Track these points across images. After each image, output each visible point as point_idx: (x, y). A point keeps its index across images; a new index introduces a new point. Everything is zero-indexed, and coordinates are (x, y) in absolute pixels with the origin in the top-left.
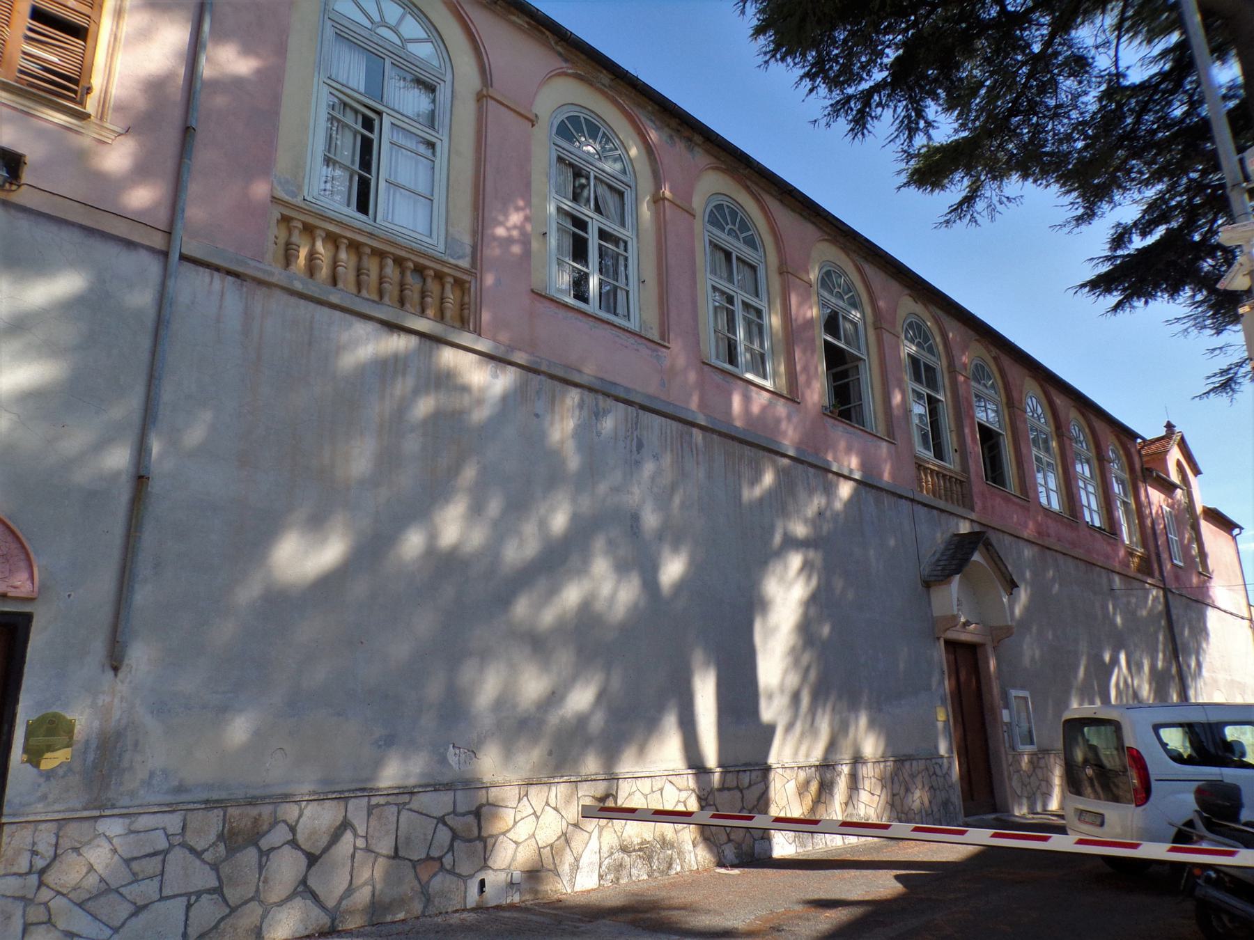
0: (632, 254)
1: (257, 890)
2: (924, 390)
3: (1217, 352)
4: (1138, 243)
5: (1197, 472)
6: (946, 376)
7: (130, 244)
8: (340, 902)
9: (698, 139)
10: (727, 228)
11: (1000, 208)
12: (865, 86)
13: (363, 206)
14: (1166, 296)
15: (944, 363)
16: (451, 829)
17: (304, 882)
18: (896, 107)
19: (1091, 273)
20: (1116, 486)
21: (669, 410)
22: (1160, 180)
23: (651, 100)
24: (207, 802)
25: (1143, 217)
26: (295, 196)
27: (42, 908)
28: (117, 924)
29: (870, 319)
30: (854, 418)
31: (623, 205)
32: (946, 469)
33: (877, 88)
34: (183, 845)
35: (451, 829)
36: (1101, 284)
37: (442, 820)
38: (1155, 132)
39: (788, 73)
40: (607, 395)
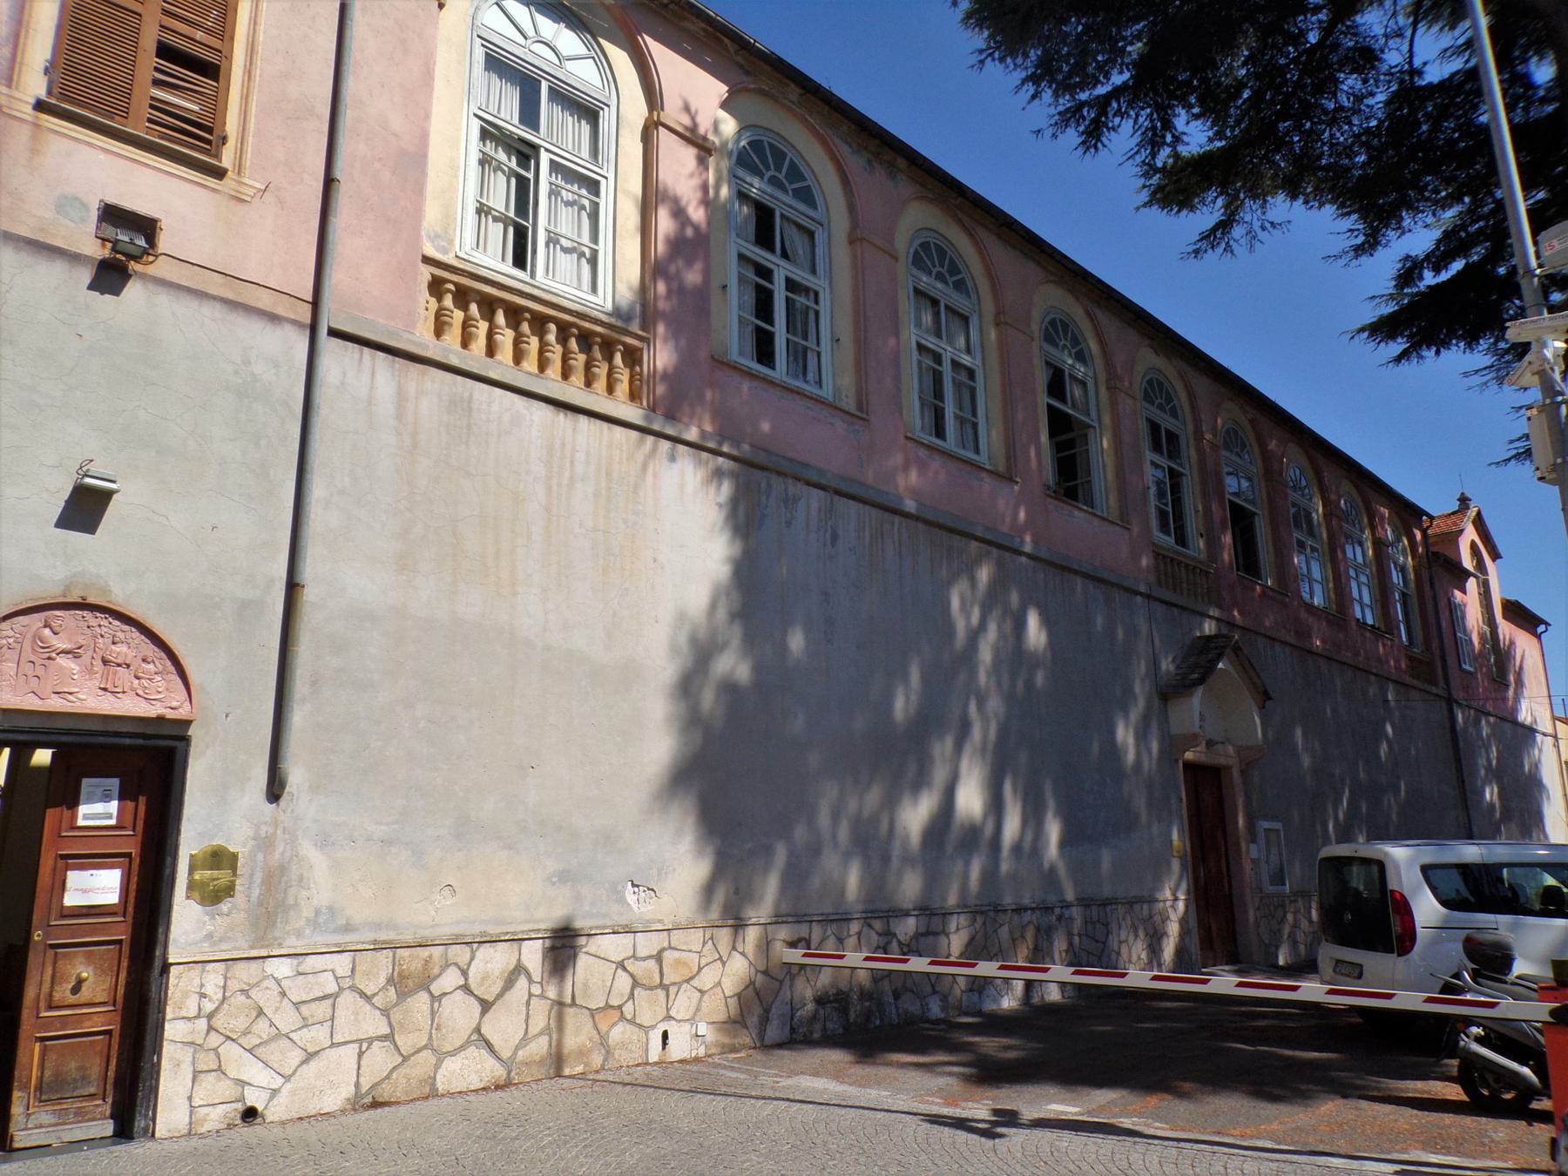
0: (824, 307)
1: (430, 1038)
2: (1164, 462)
4: (1429, 279)
6: (1192, 442)
7: (274, 318)
8: (515, 1053)
9: (901, 163)
10: (934, 271)
11: (1261, 235)
12: (1101, 90)
13: (520, 261)
14: (1462, 344)
15: (1190, 427)
16: (632, 975)
17: (478, 1030)
18: (1137, 116)
19: (1371, 313)
20: (1394, 573)
21: (852, 490)
22: (1460, 200)
23: (847, 118)
24: (375, 942)
25: (1438, 247)
26: (445, 252)
27: (212, 1055)
28: (289, 1072)
29: (1102, 377)
30: (1080, 496)
31: (813, 246)
32: (1184, 555)
33: (1117, 92)
34: (353, 988)
35: (632, 975)
36: (1383, 329)
37: (621, 965)
38: (1457, 141)
39: (1005, 78)
40: (797, 479)
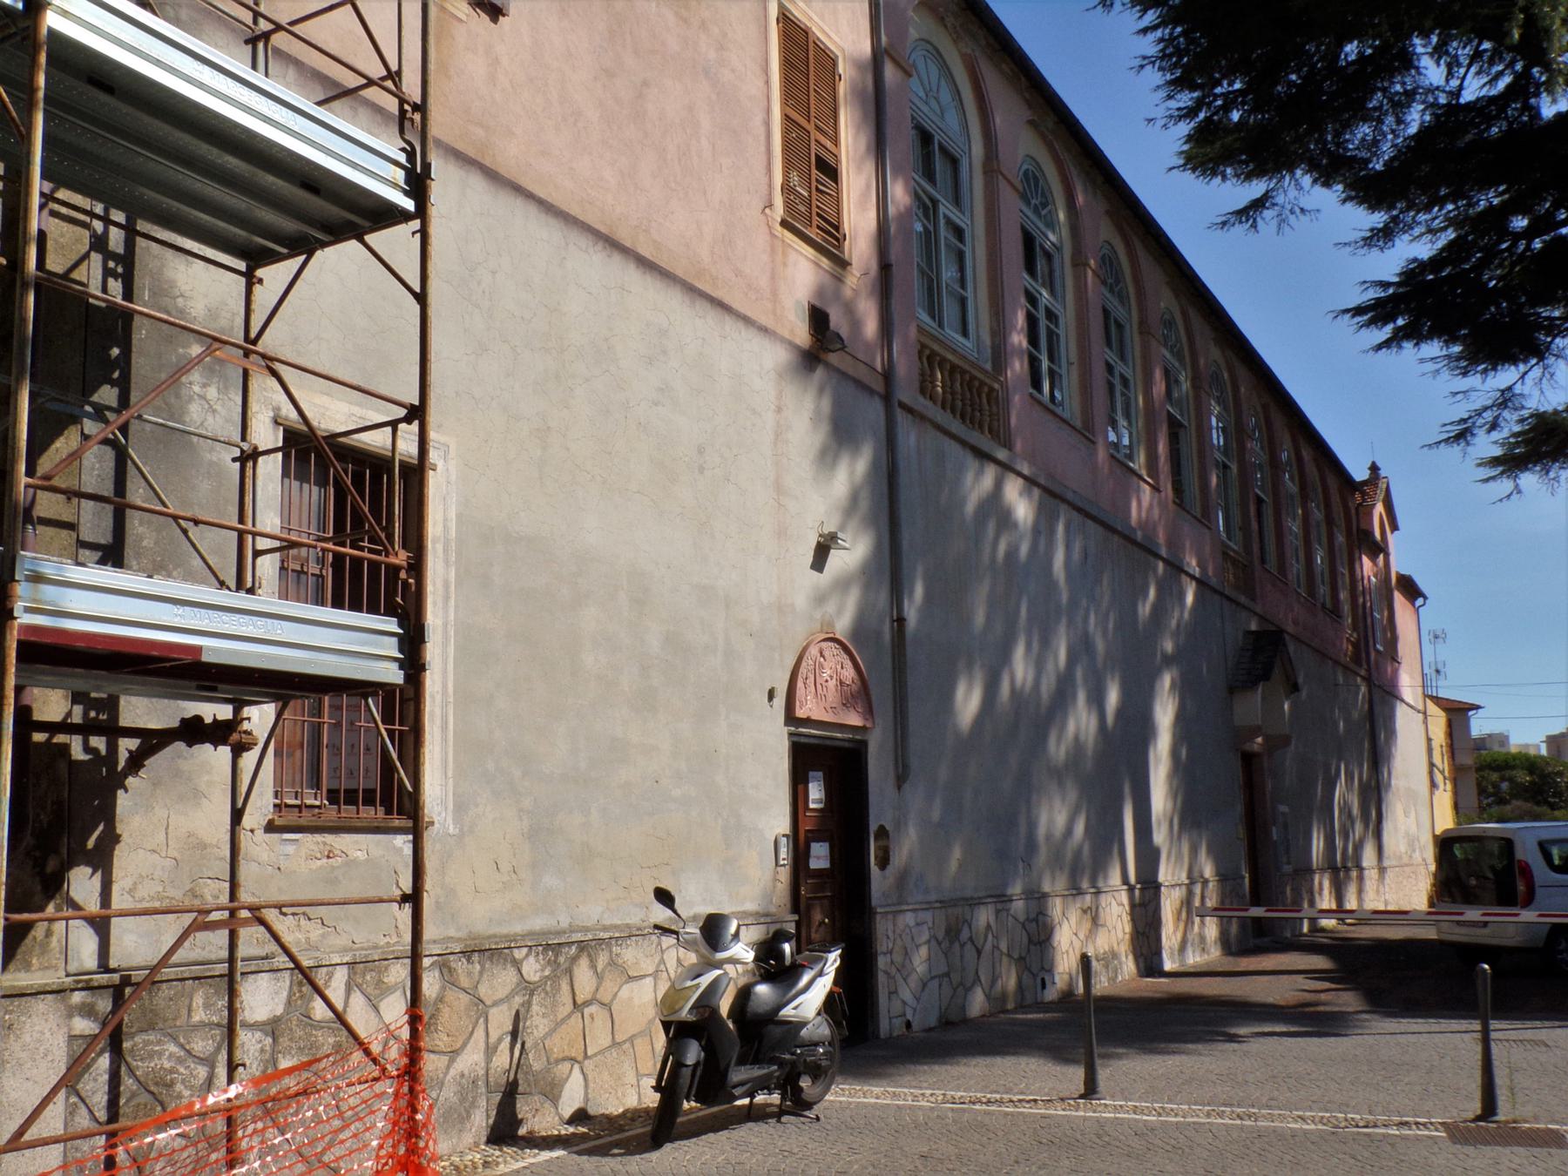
3: (1460, 397)
5: (1395, 527)
11: (1292, 218)
